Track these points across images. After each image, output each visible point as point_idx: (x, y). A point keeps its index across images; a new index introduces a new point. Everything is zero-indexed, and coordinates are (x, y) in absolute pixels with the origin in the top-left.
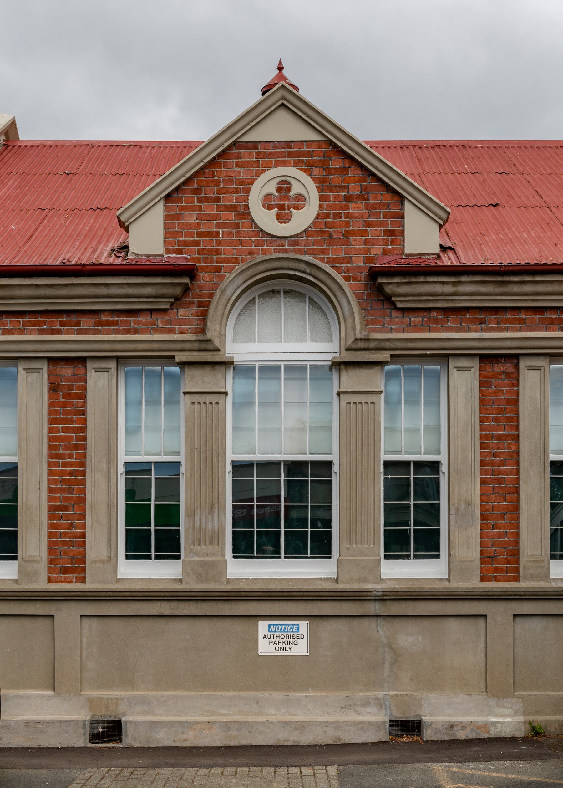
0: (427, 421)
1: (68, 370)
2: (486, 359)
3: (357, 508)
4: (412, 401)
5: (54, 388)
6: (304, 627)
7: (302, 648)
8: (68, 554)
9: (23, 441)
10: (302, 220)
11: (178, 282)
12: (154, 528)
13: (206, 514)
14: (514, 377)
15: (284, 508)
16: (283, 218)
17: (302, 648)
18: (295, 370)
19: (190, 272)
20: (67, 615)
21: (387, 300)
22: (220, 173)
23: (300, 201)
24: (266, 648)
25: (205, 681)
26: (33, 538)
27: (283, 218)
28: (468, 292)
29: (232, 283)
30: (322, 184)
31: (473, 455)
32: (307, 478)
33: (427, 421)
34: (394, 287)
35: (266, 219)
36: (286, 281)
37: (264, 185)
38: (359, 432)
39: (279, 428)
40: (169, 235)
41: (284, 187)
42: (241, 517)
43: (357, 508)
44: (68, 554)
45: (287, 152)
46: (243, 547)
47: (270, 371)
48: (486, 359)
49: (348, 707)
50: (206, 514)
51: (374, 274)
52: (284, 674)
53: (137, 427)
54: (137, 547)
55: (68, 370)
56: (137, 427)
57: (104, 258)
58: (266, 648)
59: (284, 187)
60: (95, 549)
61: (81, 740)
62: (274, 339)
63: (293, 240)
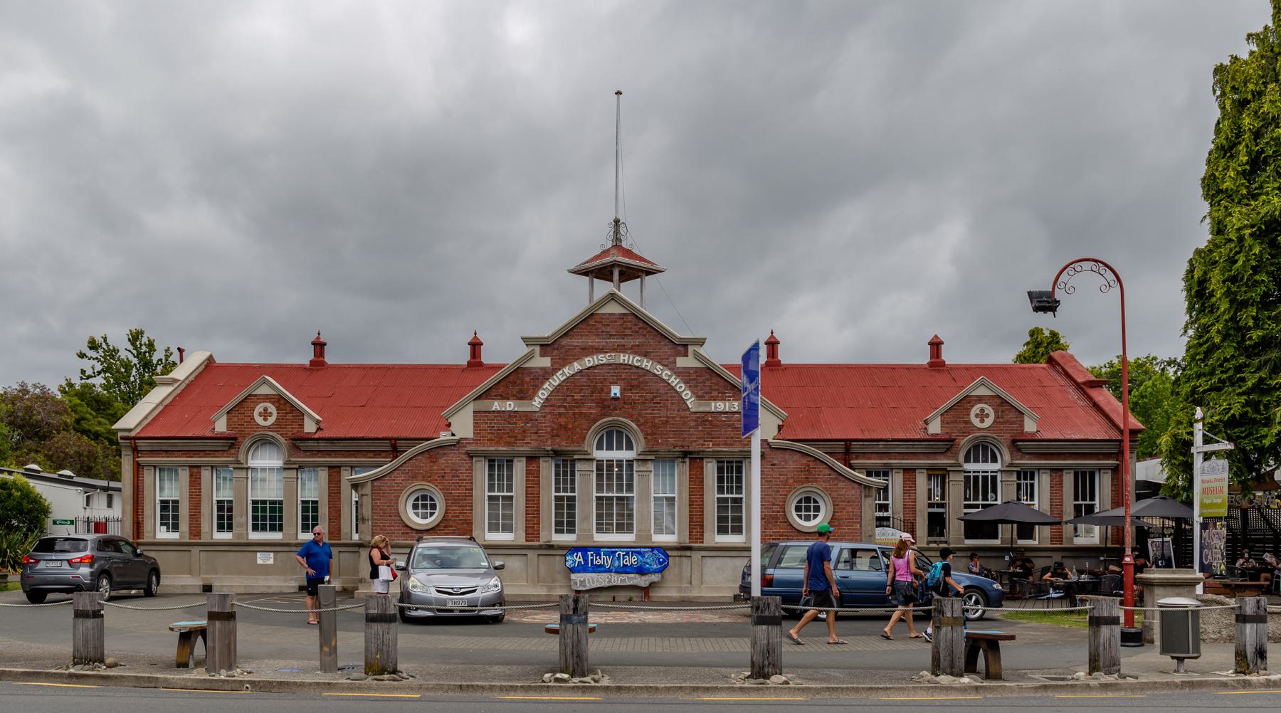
0: (313, 488)
1: (195, 470)
2: (330, 467)
3: (292, 516)
4: (310, 480)
5: (191, 475)
6: (272, 555)
7: (271, 562)
8: (195, 530)
9: (181, 492)
10: (988, 422)
11: (230, 442)
12: (225, 523)
13: (243, 518)
14: (1061, 477)
15: (268, 515)
16: (265, 419)
17: (271, 562)
18: (271, 469)
19: (235, 439)
20: (195, 550)
21: (1019, 450)
22: (245, 405)
23: (271, 414)
24: (259, 562)
25: (240, 572)
26: (184, 525)
27: (265, 419)
28: (323, 446)
29: (247, 443)
30: (278, 409)
31: (326, 499)
32: (277, 506)
33: (313, 488)
34: (298, 444)
35: (260, 420)
36: (264, 441)
37: (259, 408)
38: (291, 490)
39: (271, 490)
40: (229, 425)
41: (265, 409)
42: (255, 518)
43: (292, 516)
44: (195, 530)
45: (266, 398)
46: (255, 528)
47: (263, 470)
48: (330, 467)
49: (286, 581)
50: (243, 518)
51: (1014, 441)
52: (265, 569)
53: (219, 490)
54: (221, 528)
55: (195, 470)
56: (219, 490)
57: (209, 434)
58: (259, 562)
59: (265, 409)
60: (205, 527)
61: (199, 591)
62: (267, 461)
63: (269, 427)
